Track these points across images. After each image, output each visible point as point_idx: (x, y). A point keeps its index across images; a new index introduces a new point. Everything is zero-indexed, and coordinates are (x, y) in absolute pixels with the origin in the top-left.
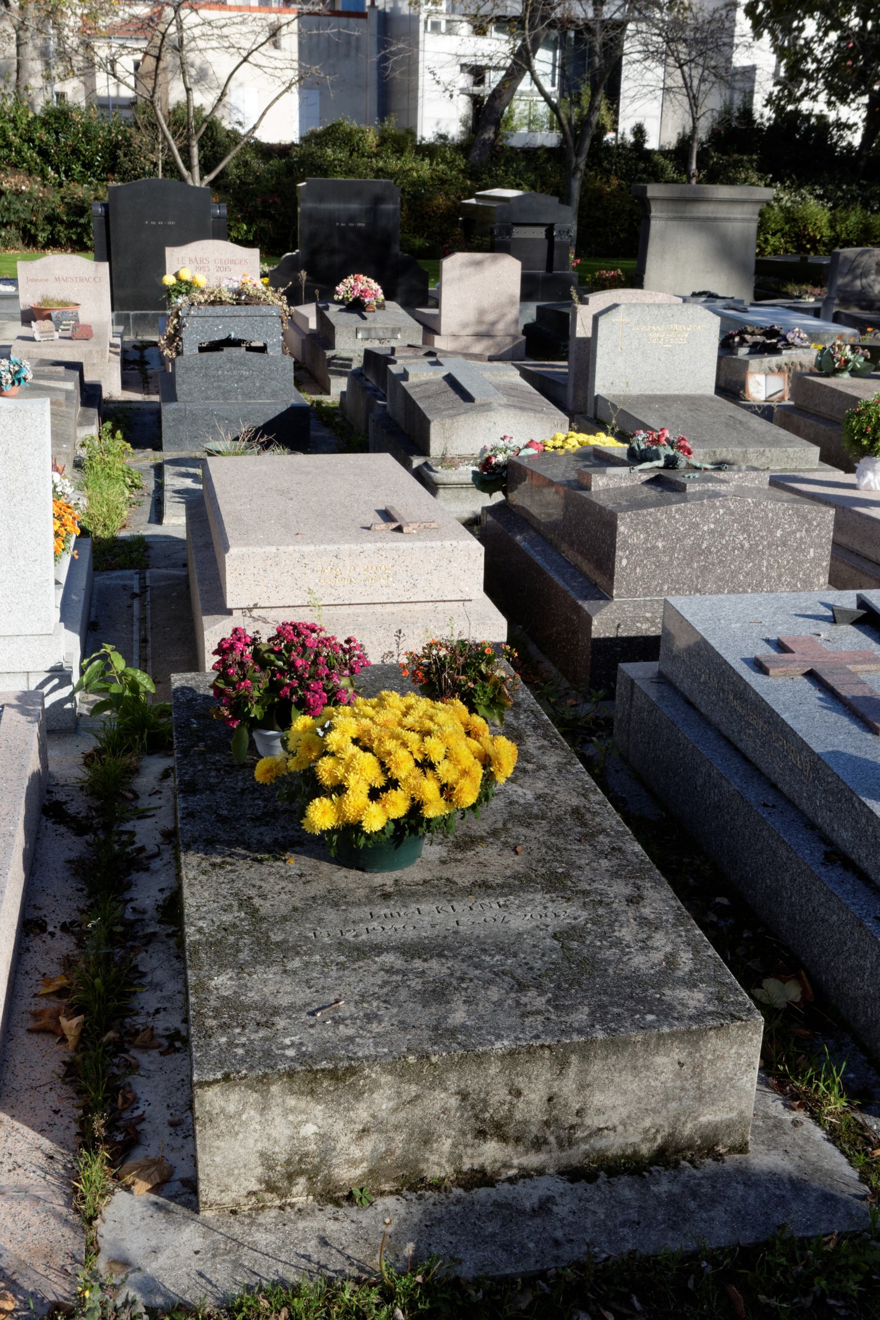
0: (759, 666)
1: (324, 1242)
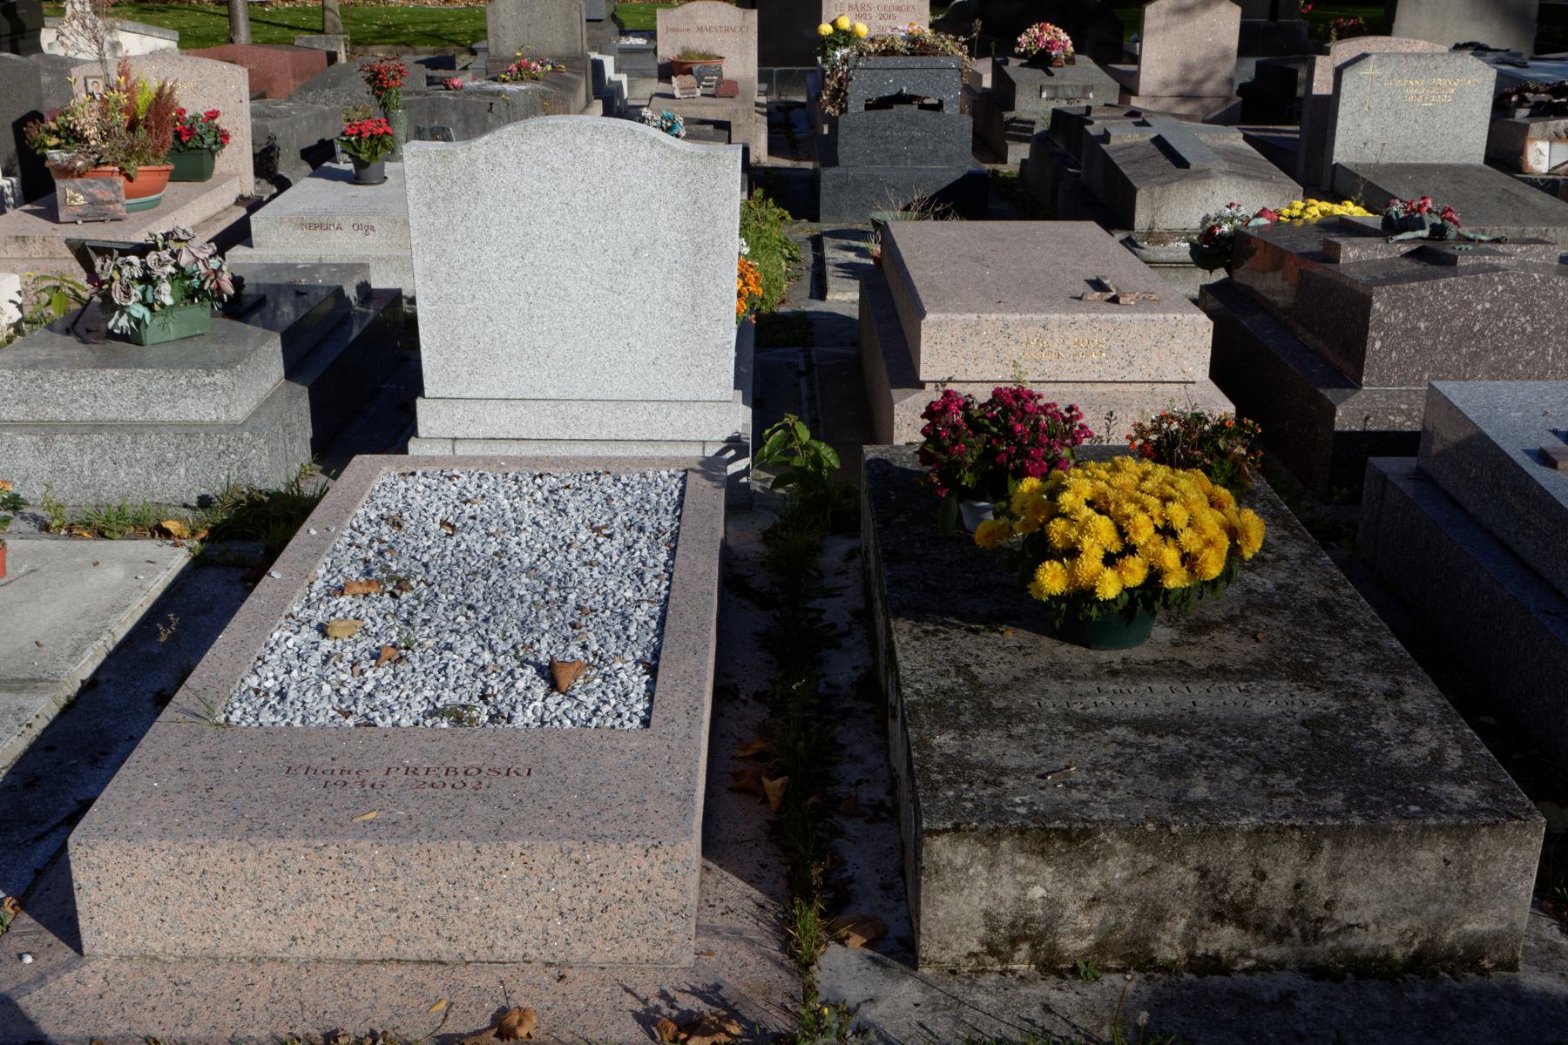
0: (1544, 458)
1: (1047, 1009)
